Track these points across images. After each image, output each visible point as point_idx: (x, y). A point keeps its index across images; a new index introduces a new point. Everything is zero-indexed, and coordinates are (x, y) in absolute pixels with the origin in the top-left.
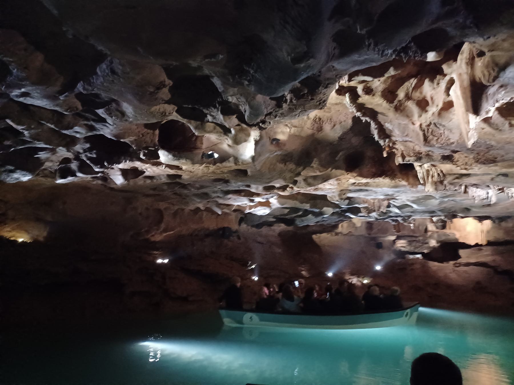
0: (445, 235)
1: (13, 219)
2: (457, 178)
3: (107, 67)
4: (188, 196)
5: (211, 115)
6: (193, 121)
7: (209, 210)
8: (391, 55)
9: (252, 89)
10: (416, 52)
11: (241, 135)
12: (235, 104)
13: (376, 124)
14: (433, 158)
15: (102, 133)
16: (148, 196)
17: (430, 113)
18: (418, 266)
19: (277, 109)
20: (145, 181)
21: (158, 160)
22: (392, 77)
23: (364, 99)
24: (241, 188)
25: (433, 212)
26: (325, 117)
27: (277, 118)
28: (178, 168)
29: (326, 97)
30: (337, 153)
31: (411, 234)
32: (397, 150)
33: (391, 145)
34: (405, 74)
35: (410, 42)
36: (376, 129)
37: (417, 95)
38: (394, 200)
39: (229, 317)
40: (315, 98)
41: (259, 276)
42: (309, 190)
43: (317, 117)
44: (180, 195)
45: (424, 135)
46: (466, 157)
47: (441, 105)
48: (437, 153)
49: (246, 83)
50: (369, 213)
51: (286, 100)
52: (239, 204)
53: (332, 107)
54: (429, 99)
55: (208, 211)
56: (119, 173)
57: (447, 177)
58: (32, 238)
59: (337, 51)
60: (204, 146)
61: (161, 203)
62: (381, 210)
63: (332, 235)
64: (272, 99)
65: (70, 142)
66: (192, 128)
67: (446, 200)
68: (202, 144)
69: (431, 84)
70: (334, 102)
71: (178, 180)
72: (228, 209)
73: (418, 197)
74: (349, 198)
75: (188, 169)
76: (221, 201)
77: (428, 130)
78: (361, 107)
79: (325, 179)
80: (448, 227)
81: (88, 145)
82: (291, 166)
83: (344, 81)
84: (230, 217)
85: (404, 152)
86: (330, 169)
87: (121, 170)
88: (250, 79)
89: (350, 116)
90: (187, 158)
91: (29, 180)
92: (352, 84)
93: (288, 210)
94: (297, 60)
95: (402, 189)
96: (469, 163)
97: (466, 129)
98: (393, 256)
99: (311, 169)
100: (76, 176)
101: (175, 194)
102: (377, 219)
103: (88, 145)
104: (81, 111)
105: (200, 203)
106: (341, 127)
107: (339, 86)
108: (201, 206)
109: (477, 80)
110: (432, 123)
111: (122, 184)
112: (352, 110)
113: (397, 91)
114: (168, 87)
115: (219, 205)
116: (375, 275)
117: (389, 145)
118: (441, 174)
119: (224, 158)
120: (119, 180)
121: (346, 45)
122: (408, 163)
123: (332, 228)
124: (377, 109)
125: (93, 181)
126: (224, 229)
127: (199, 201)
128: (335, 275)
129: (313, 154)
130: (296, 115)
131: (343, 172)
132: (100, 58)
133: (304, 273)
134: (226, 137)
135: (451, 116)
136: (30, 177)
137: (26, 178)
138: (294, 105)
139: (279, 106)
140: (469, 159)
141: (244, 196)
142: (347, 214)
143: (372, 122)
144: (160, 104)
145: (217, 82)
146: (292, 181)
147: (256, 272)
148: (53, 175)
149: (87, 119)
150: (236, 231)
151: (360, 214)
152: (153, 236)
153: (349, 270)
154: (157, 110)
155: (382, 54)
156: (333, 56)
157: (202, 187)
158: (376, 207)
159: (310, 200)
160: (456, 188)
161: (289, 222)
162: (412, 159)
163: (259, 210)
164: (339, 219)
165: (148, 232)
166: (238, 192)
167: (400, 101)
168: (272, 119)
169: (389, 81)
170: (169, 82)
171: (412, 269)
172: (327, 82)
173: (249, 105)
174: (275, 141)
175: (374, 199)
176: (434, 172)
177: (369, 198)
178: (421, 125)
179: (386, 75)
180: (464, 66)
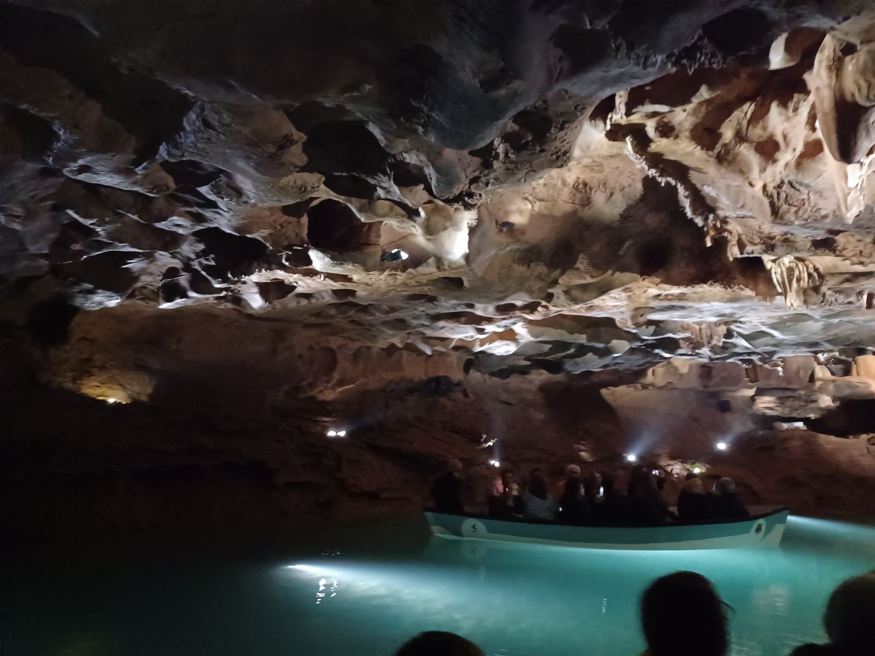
0: (850, 385)
1: (102, 368)
2: (848, 280)
3: (197, 117)
4: (372, 325)
5: (382, 187)
6: (354, 199)
7: (411, 348)
8: (664, 64)
9: (432, 139)
10: (713, 55)
11: (437, 219)
12: (415, 166)
13: (686, 189)
14: (797, 245)
15: (216, 225)
16: (309, 326)
17: (781, 164)
18: (795, 443)
19: (486, 172)
20: (298, 303)
21: (310, 267)
22: (708, 102)
23: (660, 145)
24: (459, 310)
25: (816, 344)
26: (595, 180)
27: (490, 187)
28: (345, 278)
29: (568, 145)
30: (621, 242)
31: (784, 385)
32: (731, 233)
33: (718, 224)
34: (732, 96)
35: (700, 38)
36: (686, 197)
37: (756, 133)
38: (739, 325)
39: (439, 523)
40: (546, 148)
41: (502, 460)
42: (579, 310)
43: (580, 181)
44: (360, 324)
45: (772, 204)
46: (860, 241)
47: (800, 148)
48: (803, 236)
49: (421, 129)
50: (694, 348)
51: (497, 154)
52: (461, 336)
53: (605, 163)
54: (779, 138)
55: (409, 350)
56: (256, 290)
57: (827, 278)
58: (130, 396)
59: (566, 64)
60: (384, 240)
61: (332, 339)
62: (714, 342)
63: (636, 388)
64: (472, 153)
65: (171, 241)
66: (354, 210)
67: (836, 321)
68: (380, 236)
69: (783, 110)
70: (606, 153)
71: (350, 299)
72: (444, 347)
73: (780, 317)
74: (650, 323)
75: (365, 280)
76: (429, 333)
77: (779, 194)
78: (655, 160)
79: (603, 289)
80: (854, 371)
81: (201, 247)
82: (541, 269)
83: (619, 116)
84: (450, 359)
85: (744, 237)
86: (610, 272)
87: (258, 284)
88: (425, 122)
89: (639, 177)
90: (354, 262)
91: (120, 305)
92: (635, 119)
93: (550, 346)
94: (492, 82)
95: (748, 304)
96: (866, 252)
97: (843, 190)
98: (750, 426)
99: (575, 272)
100: (187, 297)
101: (353, 321)
102: (711, 359)
103: (201, 247)
104: (176, 190)
105: (394, 336)
106: (623, 195)
107: (611, 125)
108: (397, 342)
109: (849, 98)
110: (786, 181)
111: (261, 308)
112: (640, 165)
113: (719, 128)
114: (300, 144)
115: (427, 340)
116: (715, 459)
117: (715, 226)
118: (815, 275)
119: (418, 260)
120: (256, 302)
121: (581, 53)
122: (752, 256)
123: (635, 376)
124: (687, 162)
125: (219, 304)
126: (438, 380)
127: (390, 332)
128: (641, 458)
129: (577, 245)
130: (519, 180)
131: (636, 275)
132: (185, 105)
133: (583, 454)
134: (413, 224)
135: (821, 167)
136: (119, 301)
137: (113, 302)
138: (512, 162)
139: (487, 165)
140: (866, 245)
141: (466, 323)
142: (657, 351)
143: (679, 185)
144: (291, 172)
145: (375, 130)
146: (544, 295)
147: (497, 452)
148: (154, 296)
149: (188, 203)
150: (459, 384)
151: (680, 351)
152: (321, 391)
153: (668, 451)
154: (292, 184)
155: (645, 63)
156: (560, 73)
157: (393, 309)
158: (704, 337)
159: (586, 327)
160: (850, 300)
161: (554, 367)
162: (758, 248)
163: (499, 347)
164: (647, 360)
165: (312, 385)
166: (455, 317)
167: (725, 145)
168: (481, 189)
169: (704, 109)
170: (300, 136)
171: (786, 448)
172: (561, 120)
173: (433, 166)
174: (507, 227)
175: (699, 324)
176: (801, 270)
177: (689, 321)
178: (765, 187)
179: (695, 100)
180: (824, 73)
